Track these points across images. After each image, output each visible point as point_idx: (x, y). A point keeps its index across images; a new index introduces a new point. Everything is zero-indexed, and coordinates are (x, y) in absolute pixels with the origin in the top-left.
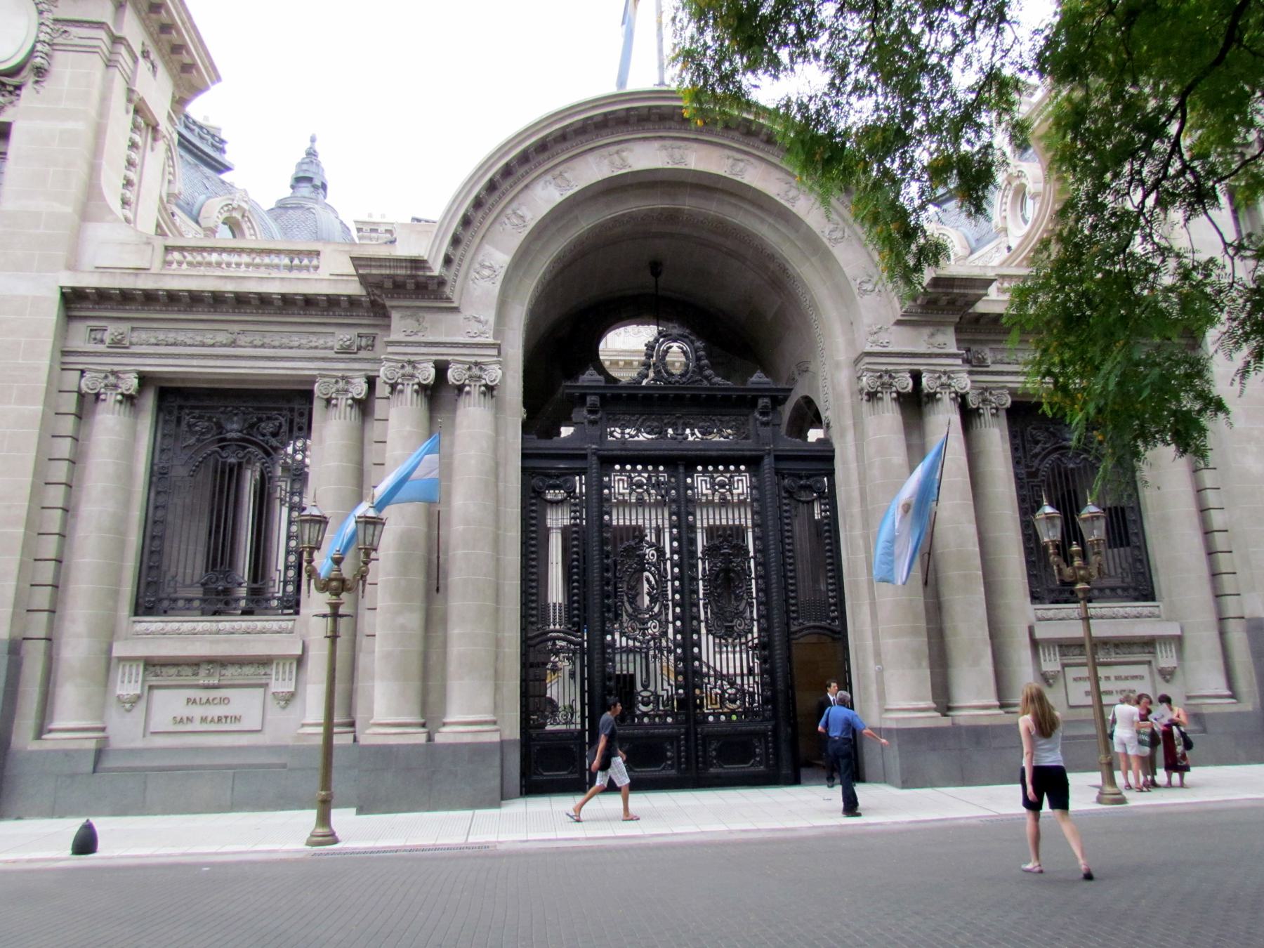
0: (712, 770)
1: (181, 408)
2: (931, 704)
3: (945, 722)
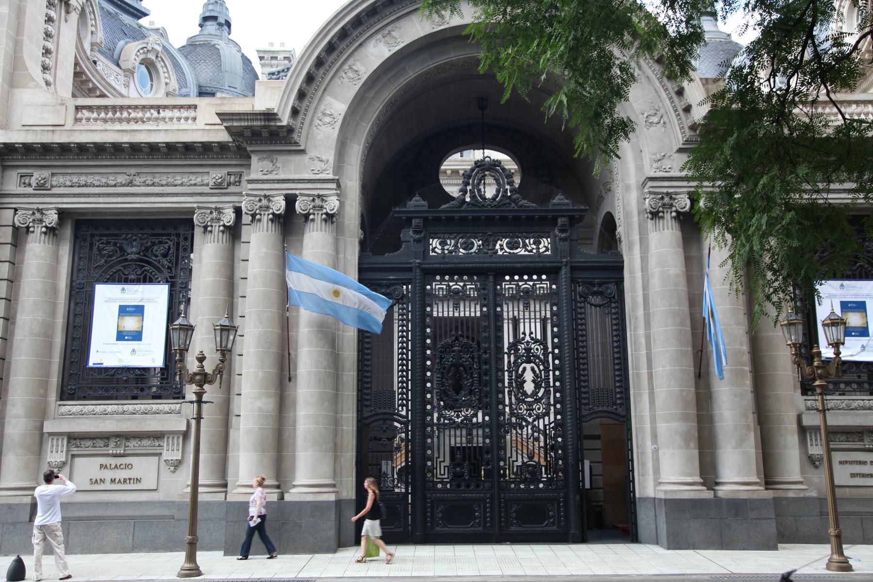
0: (513, 528)
1: (92, 236)
2: (698, 479)
3: (708, 495)
